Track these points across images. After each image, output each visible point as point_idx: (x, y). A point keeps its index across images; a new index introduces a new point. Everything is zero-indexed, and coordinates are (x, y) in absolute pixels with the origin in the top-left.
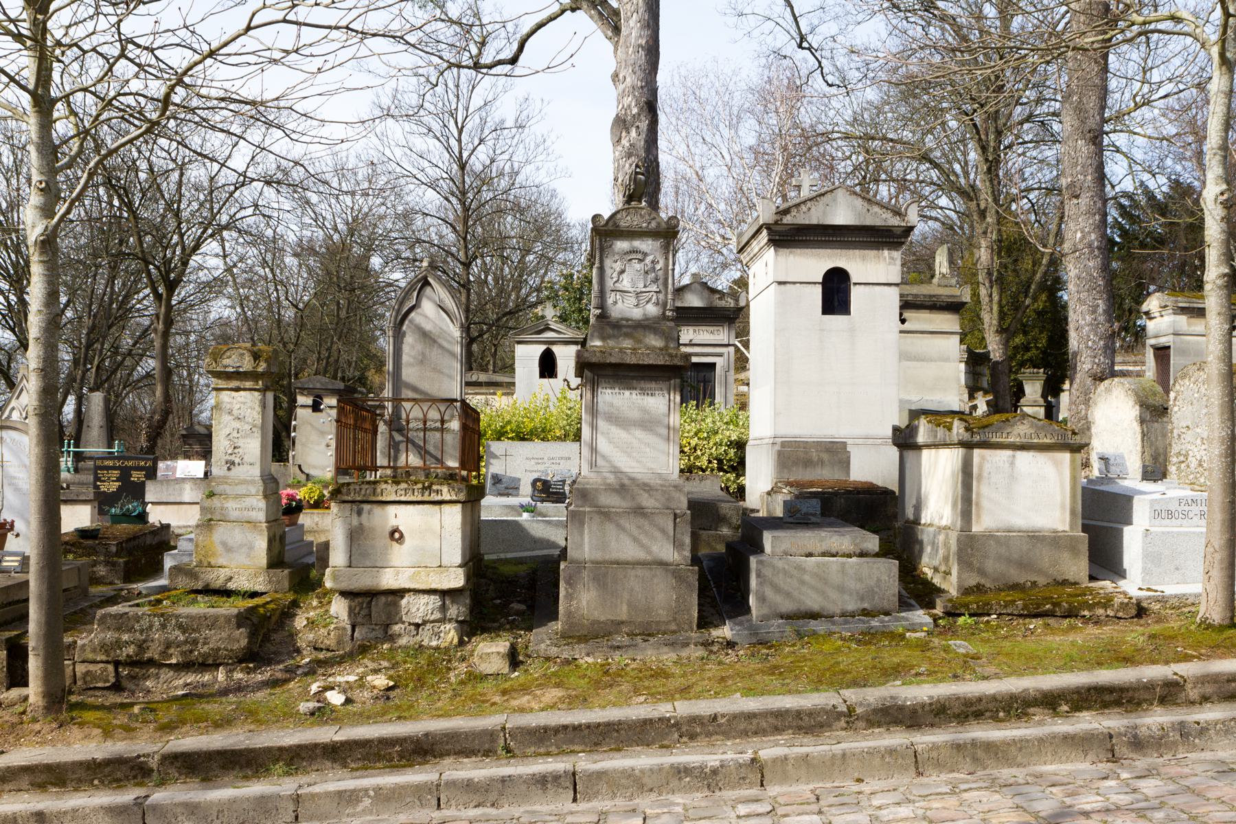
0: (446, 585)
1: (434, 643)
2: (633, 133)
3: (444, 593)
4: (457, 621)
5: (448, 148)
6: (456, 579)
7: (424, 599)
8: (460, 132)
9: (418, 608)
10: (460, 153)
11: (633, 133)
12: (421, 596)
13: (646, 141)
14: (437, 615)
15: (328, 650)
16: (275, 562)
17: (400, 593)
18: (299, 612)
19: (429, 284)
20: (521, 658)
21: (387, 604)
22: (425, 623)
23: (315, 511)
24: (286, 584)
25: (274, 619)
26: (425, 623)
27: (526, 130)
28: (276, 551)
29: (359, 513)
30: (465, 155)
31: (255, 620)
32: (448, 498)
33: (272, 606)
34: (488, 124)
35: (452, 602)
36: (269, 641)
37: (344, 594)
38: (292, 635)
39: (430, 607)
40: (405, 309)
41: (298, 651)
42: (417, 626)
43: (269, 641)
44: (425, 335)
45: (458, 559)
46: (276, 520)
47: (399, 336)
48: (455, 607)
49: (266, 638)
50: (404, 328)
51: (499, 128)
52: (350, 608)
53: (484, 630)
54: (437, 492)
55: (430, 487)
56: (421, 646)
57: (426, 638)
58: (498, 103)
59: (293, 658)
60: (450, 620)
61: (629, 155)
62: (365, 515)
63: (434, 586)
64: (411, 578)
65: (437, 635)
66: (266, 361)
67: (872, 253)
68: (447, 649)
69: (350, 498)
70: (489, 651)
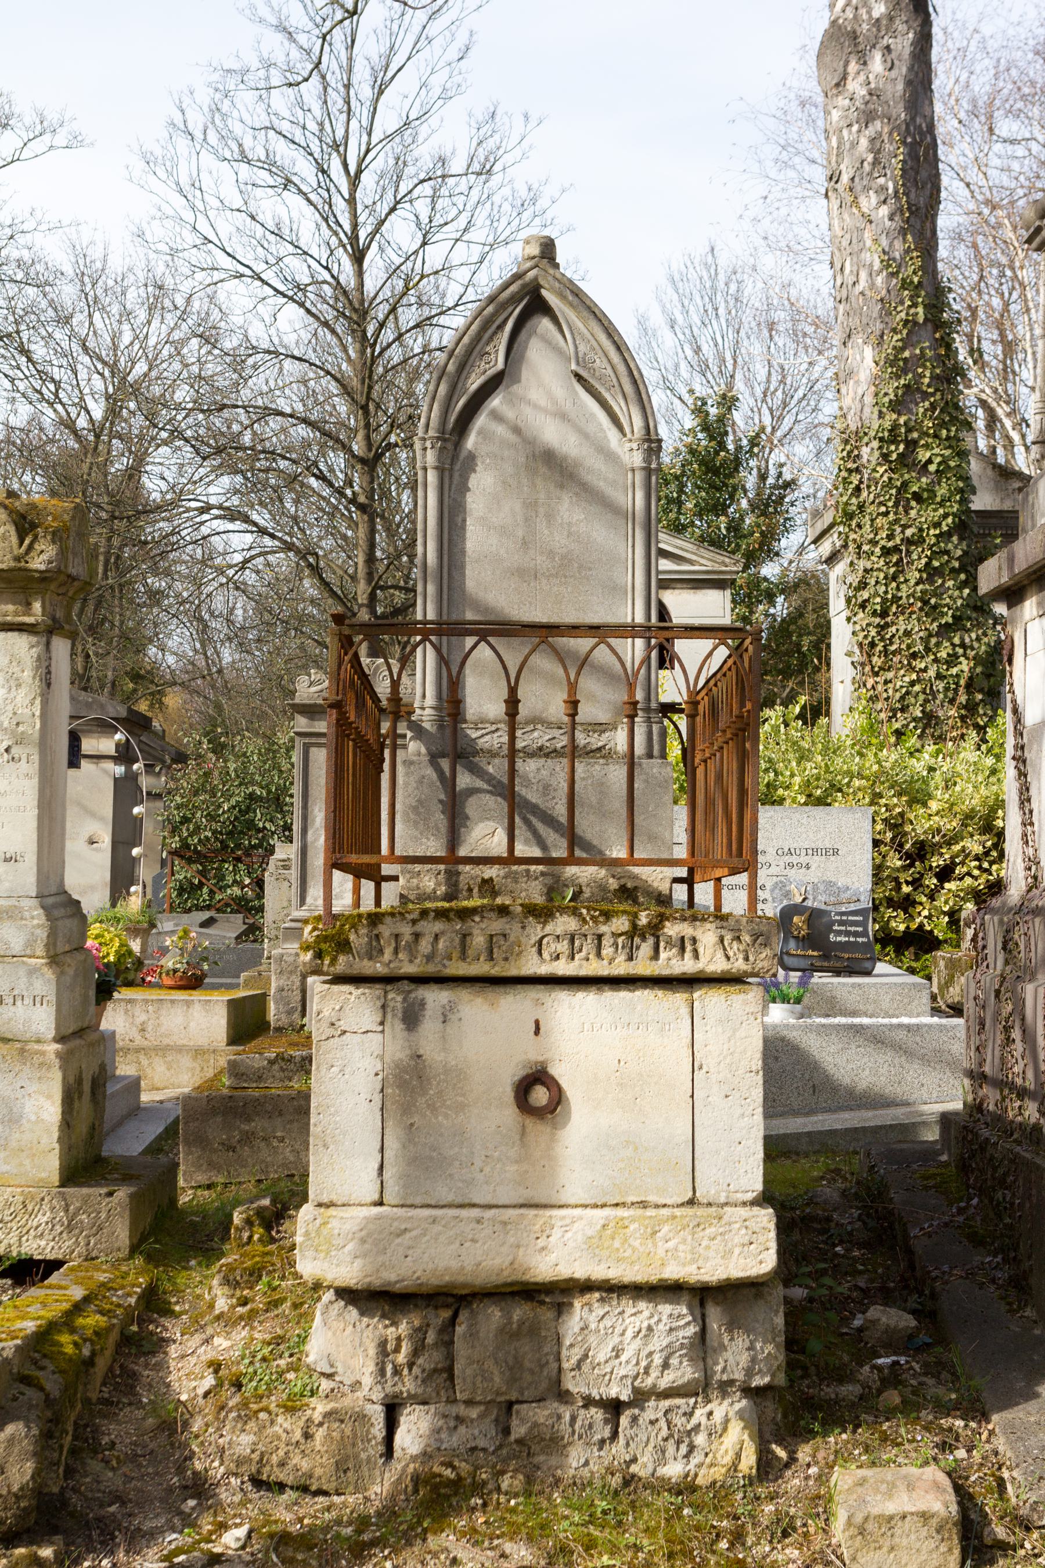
0: (715, 1269)
1: (673, 1470)
2: (877, 63)
3: (701, 1296)
4: (748, 1391)
5: (328, 218)
6: (747, 1247)
7: (638, 1315)
8: (354, 182)
9: (616, 1347)
10: (355, 226)
11: (877, 63)
12: (628, 1306)
13: (909, 83)
14: (683, 1372)
15: (304, 1489)
16: (85, 1163)
17: (560, 1293)
18: (173, 1329)
19: (546, 309)
20: (1000, 1532)
21: (509, 1334)
22: (640, 1397)
23: (196, 995)
24: (122, 1234)
25: (102, 1364)
26: (640, 1397)
27: (496, 180)
28: (82, 1128)
29: (411, 1019)
30: (363, 234)
31: (52, 1383)
32: (717, 965)
33: (91, 1321)
34: (410, 170)
35: (732, 1326)
36: (96, 1449)
37: (369, 1299)
38: (171, 1426)
39: (659, 1342)
40: (474, 383)
41: (200, 1488)
42: (614, 1408)
43: (96, 1449)
44: (551, 467)
45: (752, 1179)
46: (79, 1033)
47: (455, 468)
48: (741, 1341)
49: (87, 1444)
50: (471, 442)
51: (438, 176)
52: (383, 1350)
53: (835, 1416)
54: (681, 944)
55: (655, 928)
56: (629, 1480)
57: (646, 1450)
58: (434, 121)
59: (189, 1522)
60: (725, 1388)
61: (868, 117)
62: (429, 1026)
63: (672, 1272)
64: (593, 1245)
65: (684, 1439)
66: (56, 536)
67: (36, 803)
68: (720, 1492)
69: (379, 968)
70: (891, 1508)
